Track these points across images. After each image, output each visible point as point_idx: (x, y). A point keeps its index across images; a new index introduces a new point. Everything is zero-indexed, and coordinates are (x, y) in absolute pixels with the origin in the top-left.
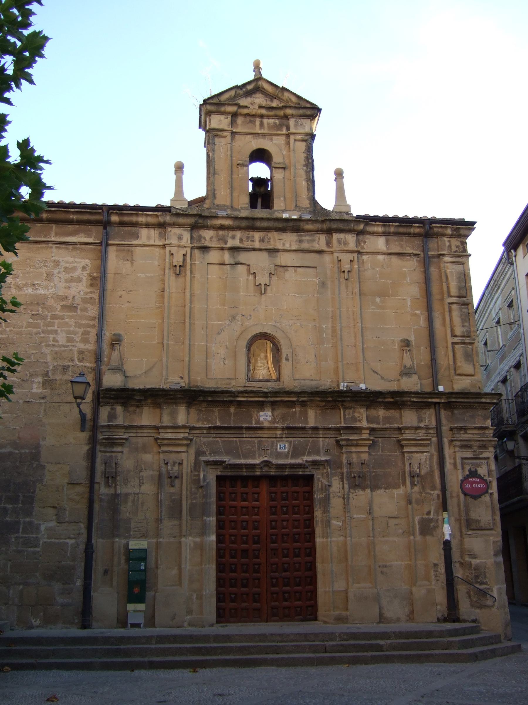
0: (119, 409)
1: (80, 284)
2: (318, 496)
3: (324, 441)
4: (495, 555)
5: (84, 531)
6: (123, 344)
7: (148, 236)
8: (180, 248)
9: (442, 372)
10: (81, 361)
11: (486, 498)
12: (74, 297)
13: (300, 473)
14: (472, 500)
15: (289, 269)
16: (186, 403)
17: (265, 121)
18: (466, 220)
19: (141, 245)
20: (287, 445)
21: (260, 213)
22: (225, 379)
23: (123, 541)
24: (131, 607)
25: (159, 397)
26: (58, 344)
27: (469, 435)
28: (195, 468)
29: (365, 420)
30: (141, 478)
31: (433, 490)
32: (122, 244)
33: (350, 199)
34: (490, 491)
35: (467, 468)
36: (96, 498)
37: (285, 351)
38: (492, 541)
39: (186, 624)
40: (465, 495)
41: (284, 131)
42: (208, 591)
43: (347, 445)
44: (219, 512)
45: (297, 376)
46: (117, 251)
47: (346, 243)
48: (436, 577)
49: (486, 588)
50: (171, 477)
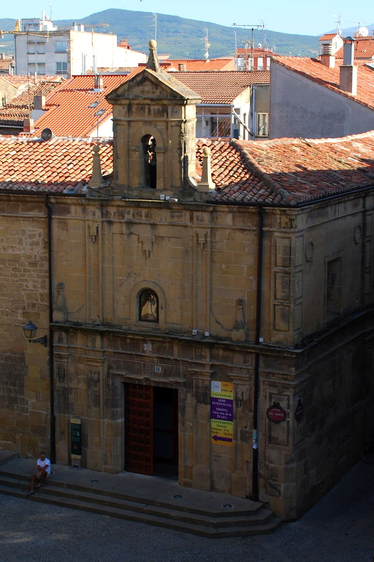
1: (38, 247)
7: (75, 211)
10: (42, 301)
11: (284, 424)
12: (35, 256)
14: (274, 423)
20: (160, 368)
24: (73, 456)
29: (208, 357)
39: (103, 470)
40: (270, 419)
45: (168, 321)
46: (58, 223)
47: (202, 220)
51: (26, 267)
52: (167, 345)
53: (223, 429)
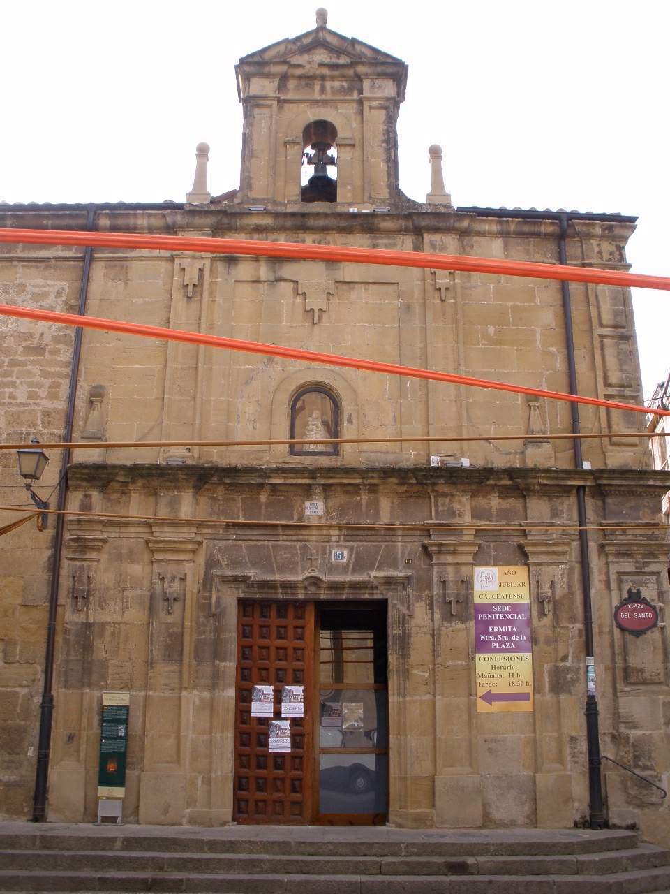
0: (95, 495)
3: (404, 547)
5: (41, 676)
6: (105, 399)
8: (195, 260)
13: (367, 596)
15: (356, 286)
16: (194, 487)
17: (328, 84)
18: (623, 214)
20: (345, 553)
22: (254, 451)
23: (97, 693)
24: (103, 791)
26: (15, 401)
27: (630, 537)
28: (205, 586)
30: (125, 600)
31: (573, 623)
32: (113, 258)
33: (448, 188)
34: (660, 624)
35: (626, 587)
36: (59, 628)
37: (347, 408)
38: (661, 702)
39: (185, 821)
40: (622, 629)
41: (355, 96)
42: (219, 773)
43: (439, 553)
48: (573, 757)
49: (651, 776)
50: (168, 599)
51: (18, 357)
52: (364, 498)
53: (506, 673)
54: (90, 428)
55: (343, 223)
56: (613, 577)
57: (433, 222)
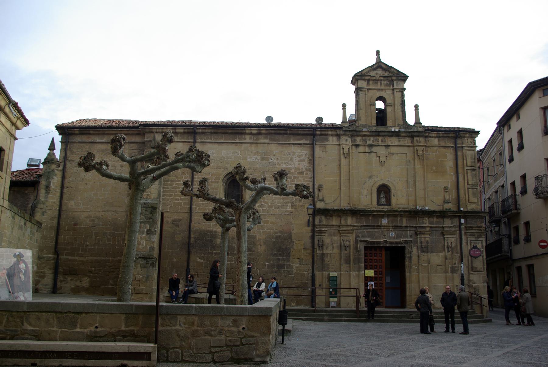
0: (323, 218)
2: (407, 255)
3: (410, 232)
4: (483, 282)
5: (311, 268)
7: (332, 140)
9: (462, 202)
11: (481, 258)
17: (383, 82)
19: (330, 144)
21: (381, 128)
23: (327, 273)
24: (331, 299)
25: (339, 213)
40: (471, 256)
41: (391, 88)
44: (365, 262)
52: (399, 218)
54: (320, 197)
55: (390, 134)
56: (469, 241)
57: (417, 134)
